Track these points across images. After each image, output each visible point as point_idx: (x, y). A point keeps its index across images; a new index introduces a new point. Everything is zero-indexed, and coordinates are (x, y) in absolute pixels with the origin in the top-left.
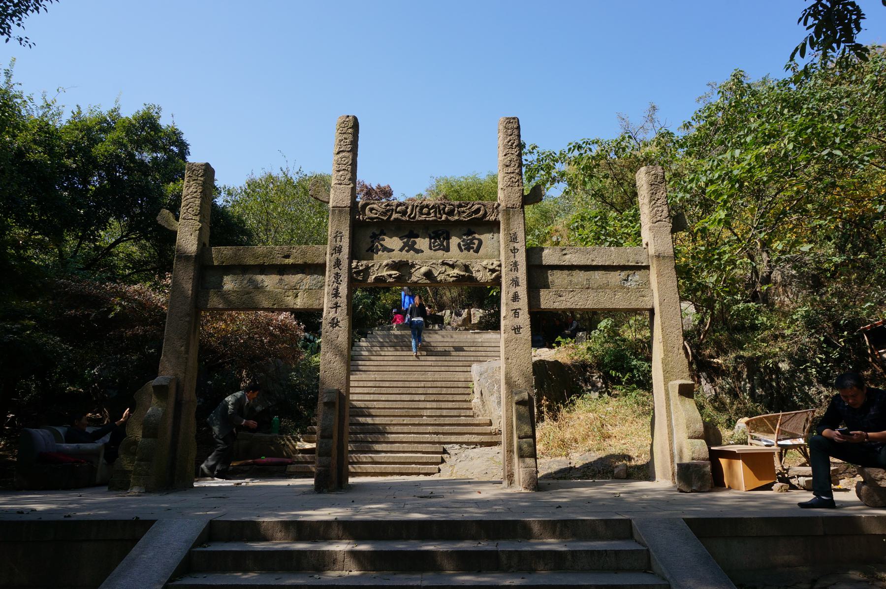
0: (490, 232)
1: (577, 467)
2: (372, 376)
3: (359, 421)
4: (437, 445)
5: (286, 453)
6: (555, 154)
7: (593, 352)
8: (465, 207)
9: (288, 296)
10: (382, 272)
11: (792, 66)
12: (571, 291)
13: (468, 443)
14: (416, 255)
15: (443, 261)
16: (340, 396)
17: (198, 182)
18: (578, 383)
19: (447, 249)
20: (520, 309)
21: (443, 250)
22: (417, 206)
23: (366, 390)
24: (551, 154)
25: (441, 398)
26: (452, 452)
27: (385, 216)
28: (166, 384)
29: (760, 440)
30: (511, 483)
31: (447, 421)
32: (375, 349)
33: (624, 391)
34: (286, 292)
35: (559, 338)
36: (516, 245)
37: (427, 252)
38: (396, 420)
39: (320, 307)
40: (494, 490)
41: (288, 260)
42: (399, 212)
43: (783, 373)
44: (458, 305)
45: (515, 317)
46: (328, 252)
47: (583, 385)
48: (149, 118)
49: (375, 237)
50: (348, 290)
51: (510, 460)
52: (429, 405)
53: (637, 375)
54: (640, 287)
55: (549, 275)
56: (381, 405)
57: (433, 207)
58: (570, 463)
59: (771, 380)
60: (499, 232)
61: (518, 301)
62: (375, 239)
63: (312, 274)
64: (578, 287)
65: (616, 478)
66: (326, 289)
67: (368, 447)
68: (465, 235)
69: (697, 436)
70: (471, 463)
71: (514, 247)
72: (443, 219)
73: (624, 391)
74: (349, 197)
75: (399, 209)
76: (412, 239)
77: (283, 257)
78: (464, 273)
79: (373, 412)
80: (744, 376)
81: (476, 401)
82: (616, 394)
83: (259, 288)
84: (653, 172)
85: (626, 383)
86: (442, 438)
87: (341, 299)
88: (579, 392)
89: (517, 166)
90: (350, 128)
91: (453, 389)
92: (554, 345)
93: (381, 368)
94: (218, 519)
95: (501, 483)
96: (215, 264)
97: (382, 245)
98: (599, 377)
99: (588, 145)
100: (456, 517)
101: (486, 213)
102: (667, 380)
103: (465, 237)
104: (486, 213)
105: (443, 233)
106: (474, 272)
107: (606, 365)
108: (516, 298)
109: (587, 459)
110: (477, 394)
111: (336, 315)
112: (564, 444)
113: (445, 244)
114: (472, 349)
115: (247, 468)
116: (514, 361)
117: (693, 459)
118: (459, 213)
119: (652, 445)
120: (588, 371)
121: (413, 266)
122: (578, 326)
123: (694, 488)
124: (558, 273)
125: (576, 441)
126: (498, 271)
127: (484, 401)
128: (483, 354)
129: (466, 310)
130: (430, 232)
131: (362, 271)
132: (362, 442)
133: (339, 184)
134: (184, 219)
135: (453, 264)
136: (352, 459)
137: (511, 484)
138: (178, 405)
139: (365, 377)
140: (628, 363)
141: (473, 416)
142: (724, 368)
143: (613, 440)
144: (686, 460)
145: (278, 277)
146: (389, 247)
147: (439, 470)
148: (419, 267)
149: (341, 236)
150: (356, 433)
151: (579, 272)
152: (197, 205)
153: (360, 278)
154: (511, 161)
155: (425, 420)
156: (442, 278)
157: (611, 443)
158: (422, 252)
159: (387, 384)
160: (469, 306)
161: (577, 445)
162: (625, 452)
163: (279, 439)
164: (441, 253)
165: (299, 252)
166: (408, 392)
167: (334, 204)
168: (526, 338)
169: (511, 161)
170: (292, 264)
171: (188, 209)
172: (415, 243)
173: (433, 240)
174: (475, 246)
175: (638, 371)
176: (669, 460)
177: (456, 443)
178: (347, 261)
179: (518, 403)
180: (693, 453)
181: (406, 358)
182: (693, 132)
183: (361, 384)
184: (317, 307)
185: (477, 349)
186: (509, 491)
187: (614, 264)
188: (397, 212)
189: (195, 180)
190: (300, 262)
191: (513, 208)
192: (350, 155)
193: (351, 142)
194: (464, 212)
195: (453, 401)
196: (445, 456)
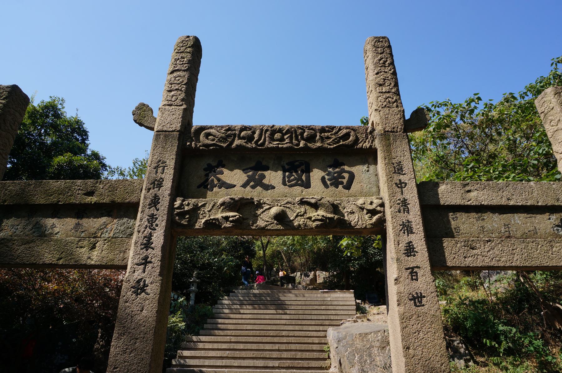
0: (363, 163)
8: (329, 131)
9: (82, 247)
10: (215, 214)
12: (488, 241)
14: (264, 192)
15: (301, 199)
19: (307, 185)
20: (418, 267)
22: (267, 130)
27: (224, 143)
32: (235, 306)
34: (79, 241)
37: (280, 188)
39: (123, 263)
41: (90, 198)
42: (243, 138)
44: (308, 268)
45: (412, 279)
46: (144, 187)
49: (211, 169)
55: (451, 219)
57: (288, 131)
60: (376, 163)
61: (414, 255)
62: (210, 172)
63: (120, 217)
66: (134, 237)
68: (330, 167)
71: (400, 180)
72: (301, 145)
74: (180, 120)
75: (243, 134)
76: (260, 172)
77: (85, 194)
78: (332, 216)
85: (504, 354)
87: (154, 252)
89: (393, 85)
90: (189, 47)
97: (219, 180)
103: (331, 170)
105: (301, 164)
106: (346, 215)
108: (410, 250)
111: (143, 275)
113: (304, 178)
114: (323, 307)
121: (260, 205)
128: (333, 312)
129: (313, 273)
131: (187, 212)
135: (316, 203)
146: (228, 182)
151: (491, 215)
153: (184, 222)
154: (384, 80)
156: (301, 223)
158: (274, 188)
160: (314, 269)
164: (298, 189)
165: (106, 187)
166: (262, 356)
167: (160, 128)
168: (432, 312)
170: (95, 203)
172: (264, 177)
173: (287, 174)
174: (345, 181)
178: (168, 198)
187: (540, 204)
188: (240, 138)
190: (107, 200)
191: (394, 132)
193: (189, 61)
194: (328, 138)
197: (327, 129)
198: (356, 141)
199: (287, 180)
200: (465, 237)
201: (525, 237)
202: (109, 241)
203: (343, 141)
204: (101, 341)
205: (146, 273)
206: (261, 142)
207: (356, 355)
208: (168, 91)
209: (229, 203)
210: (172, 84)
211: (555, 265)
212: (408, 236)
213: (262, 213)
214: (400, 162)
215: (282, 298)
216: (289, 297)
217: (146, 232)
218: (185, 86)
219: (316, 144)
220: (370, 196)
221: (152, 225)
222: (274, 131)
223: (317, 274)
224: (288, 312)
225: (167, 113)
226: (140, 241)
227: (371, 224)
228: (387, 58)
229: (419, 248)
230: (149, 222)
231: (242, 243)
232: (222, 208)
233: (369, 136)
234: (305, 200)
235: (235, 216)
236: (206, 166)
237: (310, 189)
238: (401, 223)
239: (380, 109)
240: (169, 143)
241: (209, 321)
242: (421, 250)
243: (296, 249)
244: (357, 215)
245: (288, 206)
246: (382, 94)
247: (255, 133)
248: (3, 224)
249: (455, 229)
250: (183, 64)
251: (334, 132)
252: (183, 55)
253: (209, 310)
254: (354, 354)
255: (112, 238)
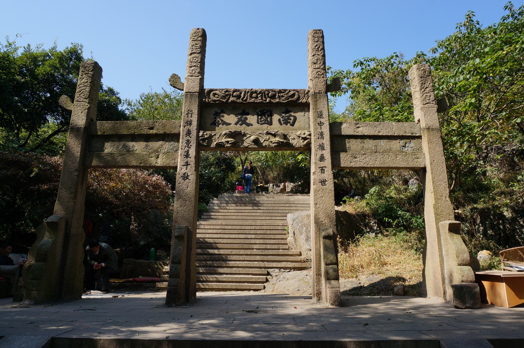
0: (302, 111)
1: (365, 286)
2: (220, 222)
3: (208, 252)
4: (263, 269)
5: (159, 273)
6: (343, 71)
7: (371, 205)
8: (283, 92)
9: (151, 157)
10: (221, 140)
11: (509, 7)
12: (364, 154)
13: (285, 268)
14: (247, 127)
16: (188, 231)
17: (89, 75)
18: (360, 227)
19: (271, 123)
21: (267, 124)
22: (248, 92)
23: (215, 231)
24: (340, 72)
25: (266, 236)
26: (274, 274)
27: (224, 99)
28: (56, 221)
29: (512, 267)
30: (319, 299)
31: (270, 252)
32: (223, 205)
33: (394, 232)
34: (150, 154)
35: (345, 198)
36: (322, 120)
37: (256, 125)
38: (235, 252)
39: (175, 165)
40: (306, 305)
41: (152, 131)
42: (235, 96)
43: (507, 219)
44: (277, 181)
45: (322, 173)
46: (182, 125)
47: (364, 228)
48: (75, 52)
49: (217, 114)
50: (196, 153)
51: (318, 282)
52: (258, 241)
53: (401, 221)
54: (414, 151)
55: (346, 142)
56: (225, 241)
57: (260, 93)
58: (360, 283)
59: (499, 224)
60: (309, 111)
61: (324, 161)
62: (217, 116)
63: (170, 141)
64: (368, 151)
65: (396, 295)
66: (180, 152)
67: (214, 270)
69: (465, 263)
70: (287, 282)
71: (320, 121)
72: (267, 101)
73: (394, 232)
74: (198, 85)
75: (235, 94)
76: (244, 116)
77: (149, 129)
78: (283, 140)
79: (219, 246)
80: (478, 222)
81: (290, 239)
82: (387, 234)
83: (129, 151)
84: (422, 68)
85: (395, 226)
86: (267, 264)
87: (191, 159)
88: (362, 233)
89: (322, 63)
90: (200, 37)
91: (274, 231)
92: (341, 203)
93: (226, 217)
94: (56, 337)
95: (310, 298)
96: (99, 134)
97: (222, 120)
98: (375, 223)
99: (367, 62)
100: (277, 336)
101: (299, 97)
102: (437, 221)
103: (284, 115)
104: (299, 97)
105: (267, 112)
106: (290, 140)
107: (380, 215)
108: (322, 158)
109: (372, 281)
110: (291, 234)
111: (186, 171)
112: (353, 269)
113: (269, 119)
114: (287, 205)
115: (129, 284)
116: (321, 206)
117: (462, 281)
118: (279, 97)
119: (424, 271)
120: (366, 219)
121: (245, 135)
122: (354, 193)
123: (468, 305)
124: (353, 141)
125: (362, 267)
126: (308, 139)
127: (296, 238)
129: (283, 184)
130: (258, 111)
131: (206, 139)
132: (210, 266)
133: (191, 76)
134: (77, 101)
135: (275, 134)
136: (203, 279)
137: (319, 300)
138: (67, 237)
139: (215, 223)
140: (395, 213)
141: (288, 249)
142: (464, 216)
143: (389, 267)
144: (457, 281)
145: (145, 143)
146: (227, 122)
147: (264, 287)
148: (249, 136)
149: (192, 113)
150: (207, 260)
152: (87, 91)
153: (205, 144)
154: (317, 60)
155: (255, 252)
156: (267, 144)
157: (388, 269)
158: (252, 125)
159: (230, 227)
160: (284, 182)
161: (364, 270)
162: (400, 276)
163: (154, 264)
164: (265, 126)
165: (160, 125)
166: (243, 233)
167: (187, 90)
168: (330, 188)
169: (317, 60)
170: (155, 134)
171: (80, 94)
172: (246, 119)
173: (260, 117)
174: (291, 121)
175: (402, 218)
176: (441, 282)
177: (277, 268)
178: (196, 131)
179: (326, 237)
180: (463, 276)
181: (243, 211)
182: (437, 55)
183: (212, 227)
184: (173, 165)
185: (290, 205)
186: (318, 306)
187: (395, 135)
188: (233, 96)
189: (86, 74)
191: (320, 93)
192: (199, 56)
193: (201, 46)
194: (283, 96)
195: (275, 239)
196: (269, 277)
197: (282, 91)
198: (299, 98)
199: (259, 120)
200: (353, 152)
201: (385, 151)
202: (166, 154)
203: (291, 98)
204: (135, 224)
205: (188, 170)
206: (245, 99)
207: (304, 227)
208: (190, 67)
209: (229, 133)
210: (191, 62)
211: (396, 166)
212: (322, 151)
213: (246, 139)
214: (322, 111)
215: (257, 199)
216: (263, 198)
217: (185, 149)
218: (199, 64)
219: (276, 100)
220: (304, 130)
221: (188, 146)
222: (252, 92)
223: (286, 185)
224: (262, 208)
225: (190, 81)
226: (183, 154)
227: (304, 145)
228: (320, 45)
229: (327, 157)
230: (186, 144)
231: (225, 160)
232: (225, 136)
233: (306, 96)
234: (269, 132)
235: (232, 141)
236: (214, 113)
237: (272, 126)
238: (319, 145)
239: (313, 79)
240: (193, 100)
241: (205, 214)
242: (328, 158)
243: (269, 165)
244: (296, 140)
245: (260, 135)
246: (315, 69)
247: (241, 94)
248: (106, 145)
249: (348, 148)
250: (197, 48)
251: (286, 93)
252: (196, 42)
253: (204, 206)
254: (303, 227)
255: (167, 152)
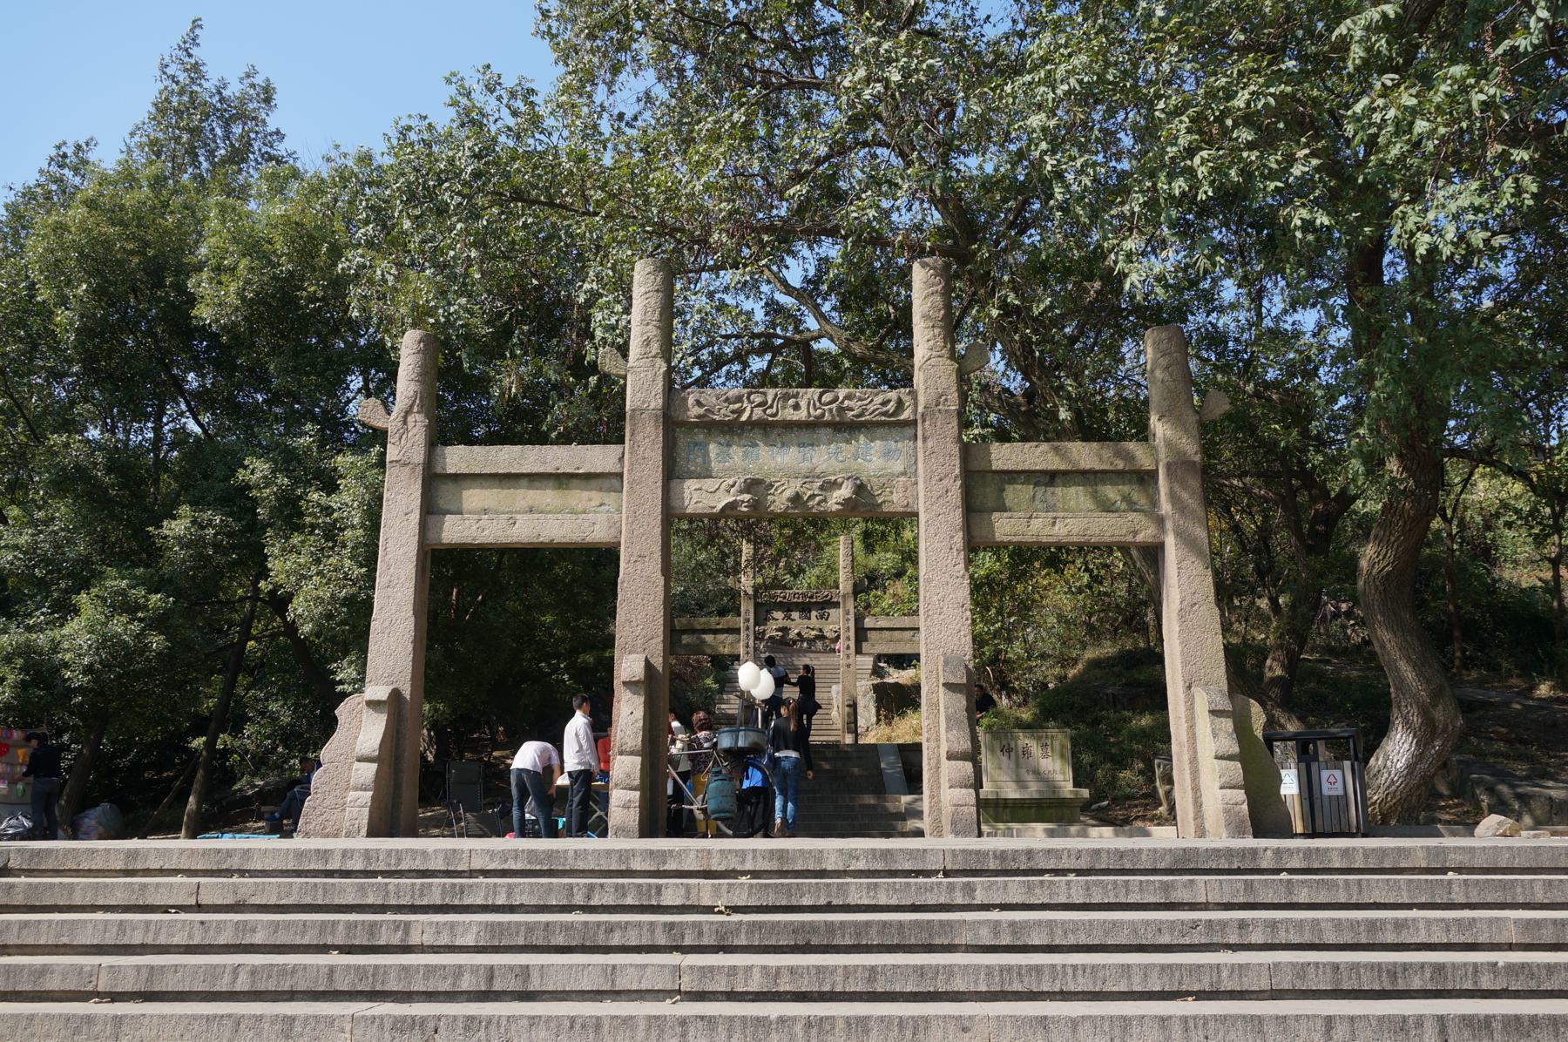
37: (798, 621)
